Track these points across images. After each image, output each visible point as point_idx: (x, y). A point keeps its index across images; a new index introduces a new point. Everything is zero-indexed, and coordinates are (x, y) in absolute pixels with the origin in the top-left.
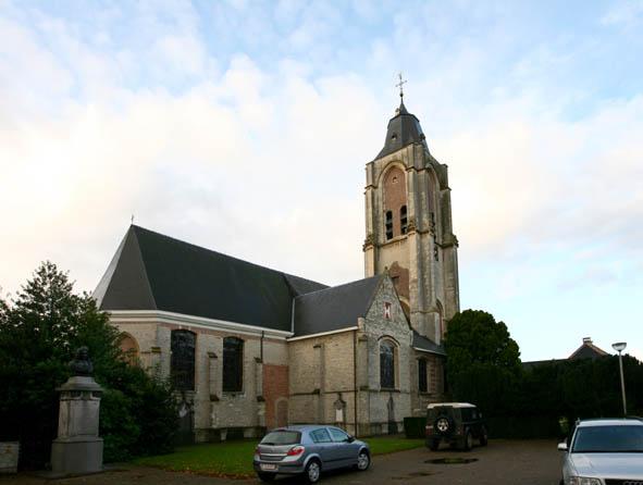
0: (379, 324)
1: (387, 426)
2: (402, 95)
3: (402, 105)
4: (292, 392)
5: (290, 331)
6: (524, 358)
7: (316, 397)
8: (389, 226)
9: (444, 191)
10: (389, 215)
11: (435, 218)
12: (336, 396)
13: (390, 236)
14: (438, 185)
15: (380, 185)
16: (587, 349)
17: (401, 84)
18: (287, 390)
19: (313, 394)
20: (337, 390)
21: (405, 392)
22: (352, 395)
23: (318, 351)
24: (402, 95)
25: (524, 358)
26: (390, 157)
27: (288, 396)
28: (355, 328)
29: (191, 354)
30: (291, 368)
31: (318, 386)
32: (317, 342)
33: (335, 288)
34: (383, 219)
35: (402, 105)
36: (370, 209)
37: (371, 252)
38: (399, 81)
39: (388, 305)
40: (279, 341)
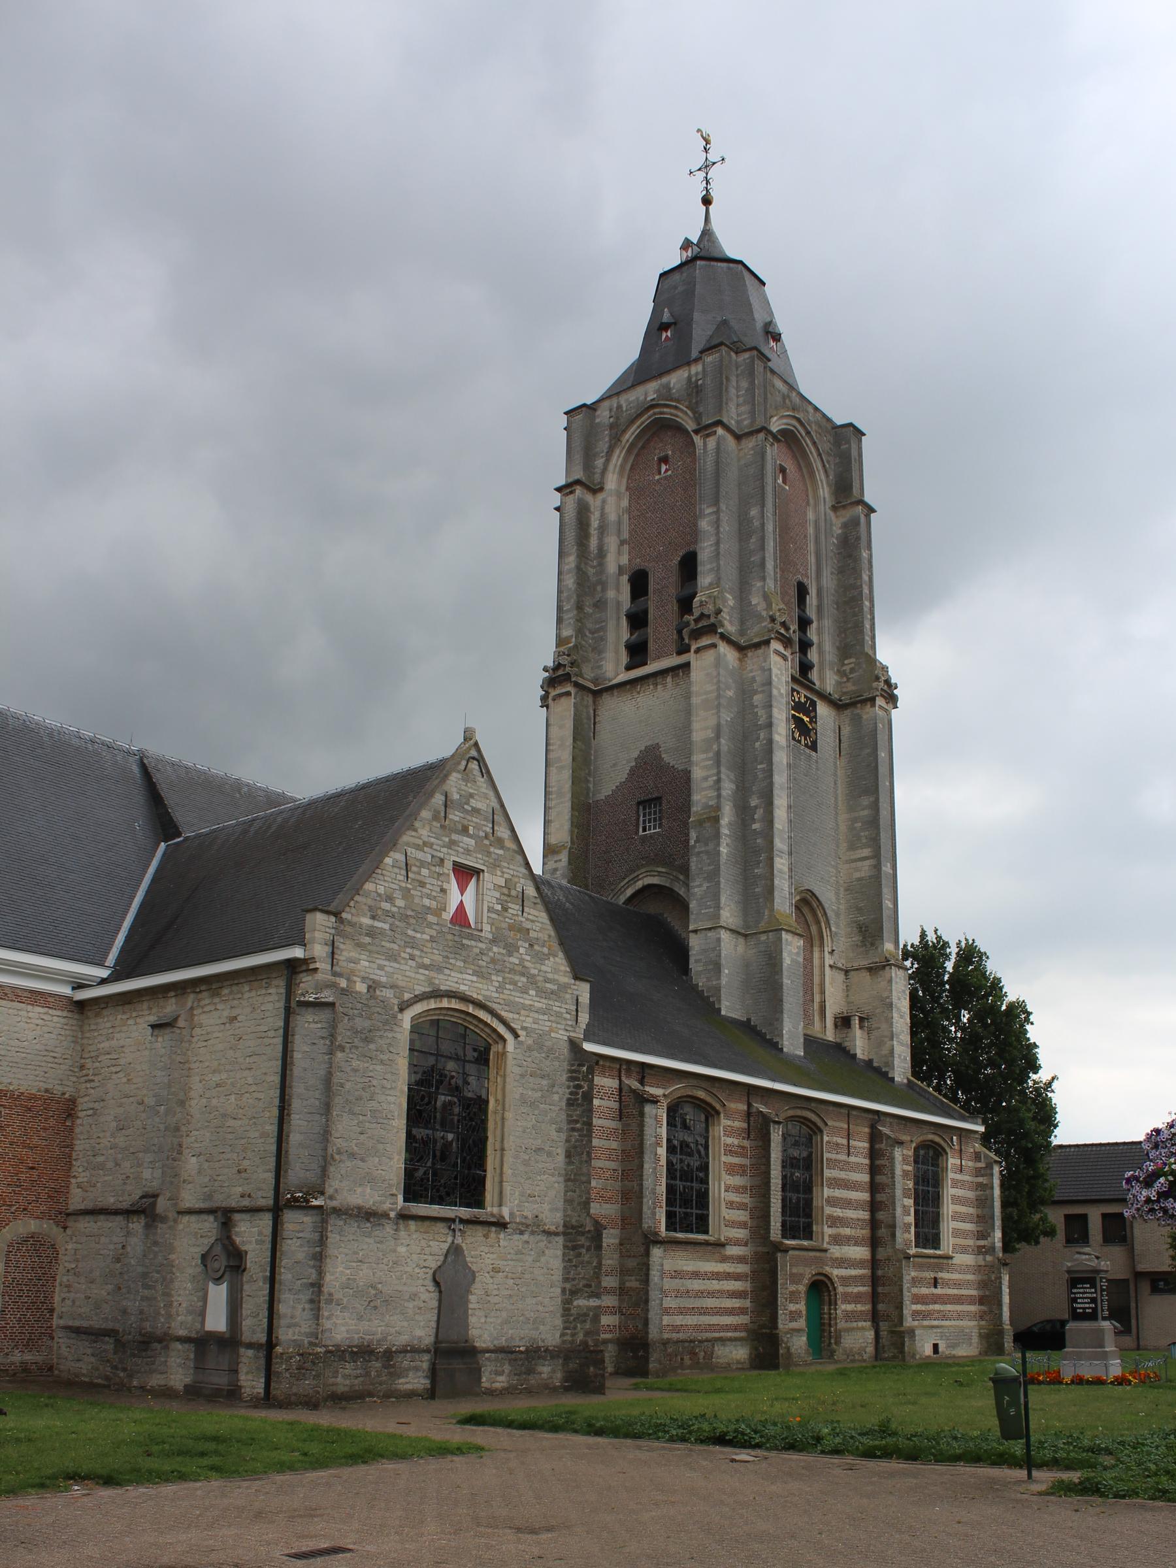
0: (412, 943)
1: (425, 1362)
2: (707, 201)
3: (707, 233)
4: (77, 1199)
5: (101, 964)
6: (1062, 1136)
7: (137, 1225)
8: (637, 620)
9: (847, 515)
10: (639, 583)
11: (812, 600)
12: (209, 1226)
13: (637, 652)
14: (825, 492)
15: (612, 482)
16: (1035, 1046)
17: (707, 166)
18: (60, 1192)
19: (128, 1213)
20: (219, 1201)
21: (533, 1227)
22: (266, 1220)
23: (163, 1042)
24: (707, 201)
25: (1062, 1136)
26: (650, 391)
27: (65, 1217)
28: (298, 952)
29: (695, 1162)
30: (83, 1103)
31: (150, 1177)
32: (170, 1007)
33: (313, 804)
34: (620, 595)
35: (707, 233)
36: (571, 560)
37: (566, 709)
38: (700, 162)
39: (465, 873)
40: (36, 997)
